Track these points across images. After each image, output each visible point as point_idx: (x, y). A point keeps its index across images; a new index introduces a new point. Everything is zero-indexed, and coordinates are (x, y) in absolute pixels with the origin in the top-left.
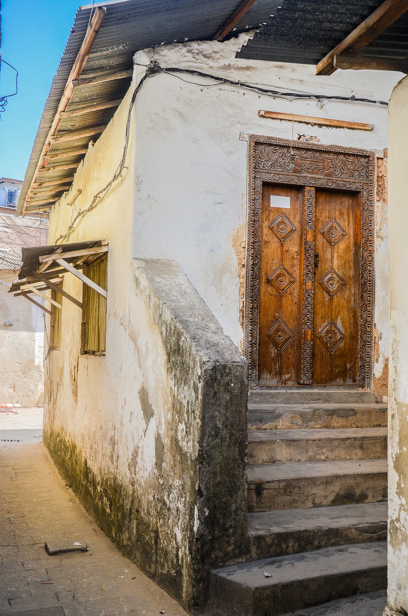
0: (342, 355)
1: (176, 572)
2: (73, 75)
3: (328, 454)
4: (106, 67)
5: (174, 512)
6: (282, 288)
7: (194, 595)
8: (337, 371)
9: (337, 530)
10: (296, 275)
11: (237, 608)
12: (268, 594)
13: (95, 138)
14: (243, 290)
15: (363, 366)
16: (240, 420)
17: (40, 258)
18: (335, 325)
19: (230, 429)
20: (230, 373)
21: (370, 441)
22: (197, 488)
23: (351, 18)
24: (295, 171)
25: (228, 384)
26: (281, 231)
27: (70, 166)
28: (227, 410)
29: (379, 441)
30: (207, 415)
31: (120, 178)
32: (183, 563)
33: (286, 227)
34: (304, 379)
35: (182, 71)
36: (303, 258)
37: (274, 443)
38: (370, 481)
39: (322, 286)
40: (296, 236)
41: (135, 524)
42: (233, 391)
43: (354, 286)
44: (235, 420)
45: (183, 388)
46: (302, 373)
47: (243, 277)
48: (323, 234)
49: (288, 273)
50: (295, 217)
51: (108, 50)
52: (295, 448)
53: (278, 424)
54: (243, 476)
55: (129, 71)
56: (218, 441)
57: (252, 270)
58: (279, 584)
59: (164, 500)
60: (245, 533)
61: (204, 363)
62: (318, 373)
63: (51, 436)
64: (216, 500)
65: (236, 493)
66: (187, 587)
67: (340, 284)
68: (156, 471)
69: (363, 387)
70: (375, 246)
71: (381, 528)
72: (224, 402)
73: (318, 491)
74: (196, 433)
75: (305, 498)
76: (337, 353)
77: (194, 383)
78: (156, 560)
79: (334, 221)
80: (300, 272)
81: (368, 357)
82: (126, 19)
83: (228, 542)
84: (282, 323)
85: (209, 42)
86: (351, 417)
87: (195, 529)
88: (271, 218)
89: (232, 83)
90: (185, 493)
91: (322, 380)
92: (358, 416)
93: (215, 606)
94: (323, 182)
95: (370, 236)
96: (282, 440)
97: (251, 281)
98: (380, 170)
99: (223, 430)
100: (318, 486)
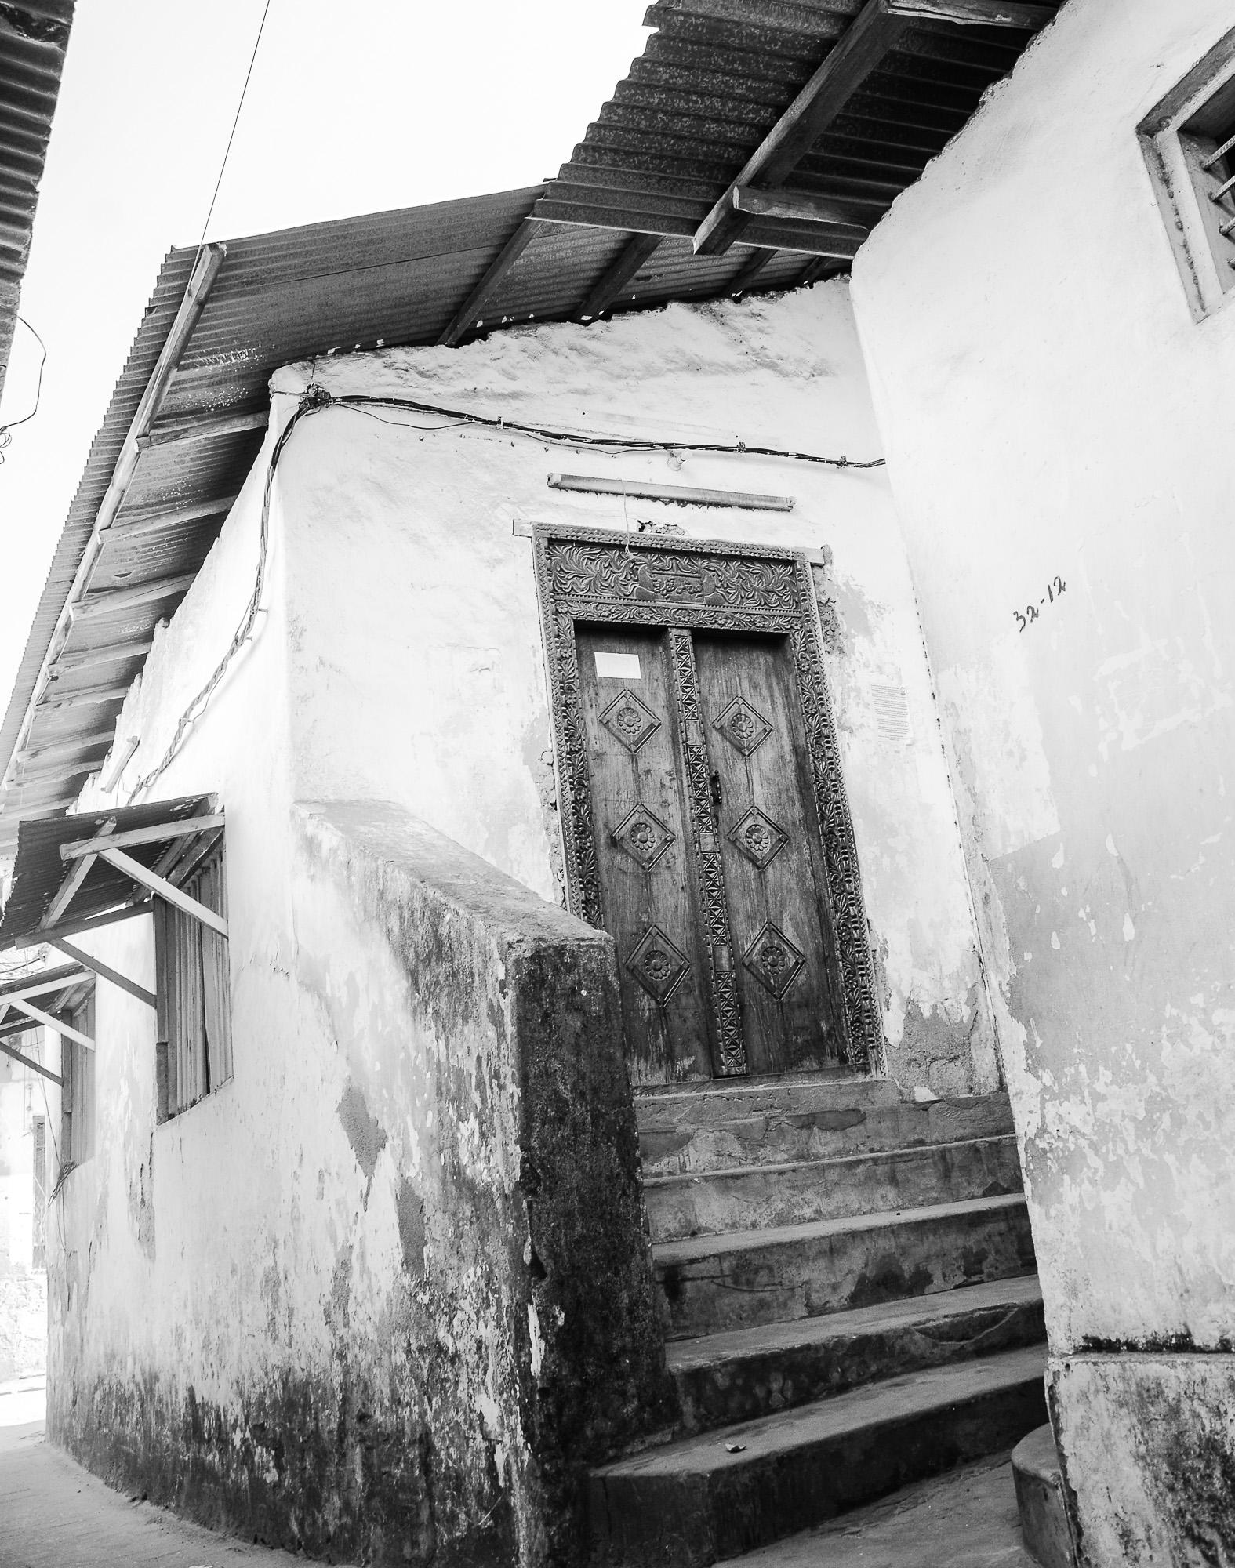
0: (805, 1004)
1: (492, 1517)
2: (139, 424)
3: (819, 1202)
4: (209, 409)
5: (471, 1358)
6: (647, 857)
7: (551, 1547)
8: (799, 1040)
9: (880, 1338)
10: (675, 824)
11: (672, 1543)
12: (745, 1484)
13: (167, 609)
14: (561, 860)
16: (613, 1079)
17: (63, 848)
18: (779, 933)
19: (592, 1101)
20: (575, 965)
21: (909, 1164)
22: (527, 1258)
23: (756, 112)
24: (642, 597)
25: (573, 990)
26: (628, 729)
27: (109, 694)
28: (578, 1055)
29: (930, 1161)
30: (533, 1070)
31: (247, 643)
32: (510, 1480)
34: (727, 1065)
35: (377, 400)
36: (685, 784)
37: (688, 1187)
38: (931, 1237)
40: (663, 737)
41: (358, 1459)
42: (587, 1008)
43: (809, 843)
45: (462, 1032)
46: (722, 1049)
47: (556, 832)
48: (721, 730)
49: (656, 820)
50: (654, 696)
51: (217, 362)
52: (739, 1195)
53: (687, 1158)
54: (637, 1217)
55: (260, 416)
57: (574, 814)
58: (768, 1455)
59: (438, 1342)
60: (661, 1365)
61: (510, 946)
62: (757, 1048)
63: (75, 1403)
64: (579, 1284)
65: (626, 1262)
66: (529, 1536)
67: (774, 840)
68: (406, 1281)
69: (867, 1071)
70: (839, 746)
71: (980, 1324)
72: (569, 1037)
73: (814, 1273)
74: (509, 1123)
75: (788, 1294)
76: (794, 999)
77: (491, 1006)
78: (432, 1514)
79: (741, 701)
80: (684, 817)
81: (866, 999)
82: (261, 283)
83: (623, 1394)
84: (658, 937)
85: (428, 348)
86: (853, 1129)
87: (536, 1368)
88: (601, 701)
89: (486, 422)
90: (494, 1292)
91: (769, 1065)
92: (870, 1124)
93: (612, 1561)
94: (704, 617)
95: (825, 726)
96: (706, 1179)
97: (576, 839)
98: (822, 589)
99: (574, 1105)
100: (815, 1260)
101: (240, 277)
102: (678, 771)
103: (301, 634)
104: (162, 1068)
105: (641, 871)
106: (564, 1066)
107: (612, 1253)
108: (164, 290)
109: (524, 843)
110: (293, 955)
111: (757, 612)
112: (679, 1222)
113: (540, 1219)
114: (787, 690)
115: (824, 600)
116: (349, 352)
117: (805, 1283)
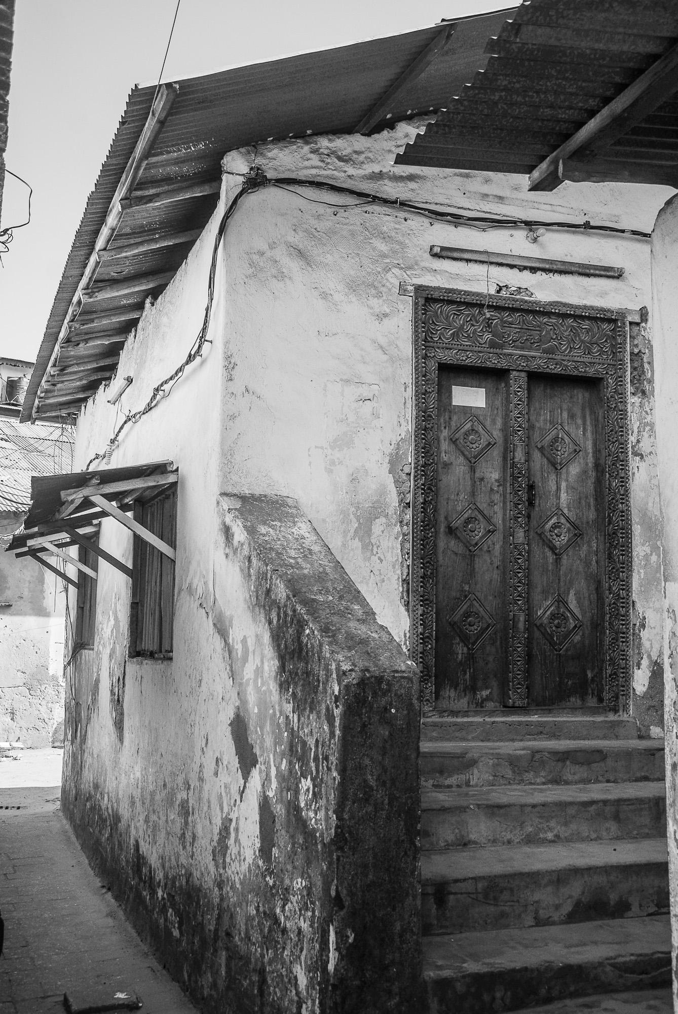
2: (120, 193)
4: (176, 178)
6: (474, 542)
8: (570, 683)
10: (498, 519)
15: (615, 674)
21: (630, 807)
22: (333, 893)
25: (386, 709)
28: (384, 754)
29: (647, 806)
31: (198, 359)
33: (479, 439)
34: (514, 699)
36: (508, 491)
38: (635, 878)
39: (541, 538)
43: (597, 538)
44: (399, 772)
45: (309, 716)
47: (407, 524)
48: (541, 450)
49: (484, 516)
50: (494, 422)
55: (215, 184)
56: (370, 809)
57: (422, 512)
61: (344, 673)
64: (366, 914)
73: (544, 896)
76: (569, 653)
79: (560, 427)
80: (505, 514)
83: (389, 992)
84: (475, 602)
85: (347, 136)
86: (595, 765)
87: (331, 967)
88: (453, 424)
90: (312, 903)
92: (610, 762)
94: (540, 362)
96: (479, 806)
99: (377, 791)
100: (546, 886)
101: (193, 99)
102: (505, 480)
103: (233, 368)
104: (134, 619)
105: (468, 552)
106: (373, 763)
107: (392, 895)
108: (133, 111)
109: (383, 532)
110: (212, 604)
111: (582, 360)
112: (456, 836)
113: (344, 869)
114: (597, 420)
115: (636, 351)
116: (284, 139)
117: (536, 902)
